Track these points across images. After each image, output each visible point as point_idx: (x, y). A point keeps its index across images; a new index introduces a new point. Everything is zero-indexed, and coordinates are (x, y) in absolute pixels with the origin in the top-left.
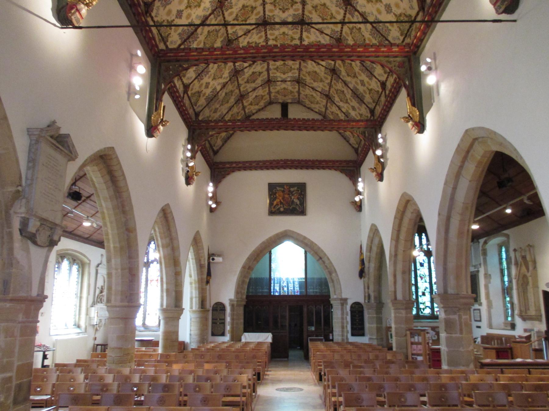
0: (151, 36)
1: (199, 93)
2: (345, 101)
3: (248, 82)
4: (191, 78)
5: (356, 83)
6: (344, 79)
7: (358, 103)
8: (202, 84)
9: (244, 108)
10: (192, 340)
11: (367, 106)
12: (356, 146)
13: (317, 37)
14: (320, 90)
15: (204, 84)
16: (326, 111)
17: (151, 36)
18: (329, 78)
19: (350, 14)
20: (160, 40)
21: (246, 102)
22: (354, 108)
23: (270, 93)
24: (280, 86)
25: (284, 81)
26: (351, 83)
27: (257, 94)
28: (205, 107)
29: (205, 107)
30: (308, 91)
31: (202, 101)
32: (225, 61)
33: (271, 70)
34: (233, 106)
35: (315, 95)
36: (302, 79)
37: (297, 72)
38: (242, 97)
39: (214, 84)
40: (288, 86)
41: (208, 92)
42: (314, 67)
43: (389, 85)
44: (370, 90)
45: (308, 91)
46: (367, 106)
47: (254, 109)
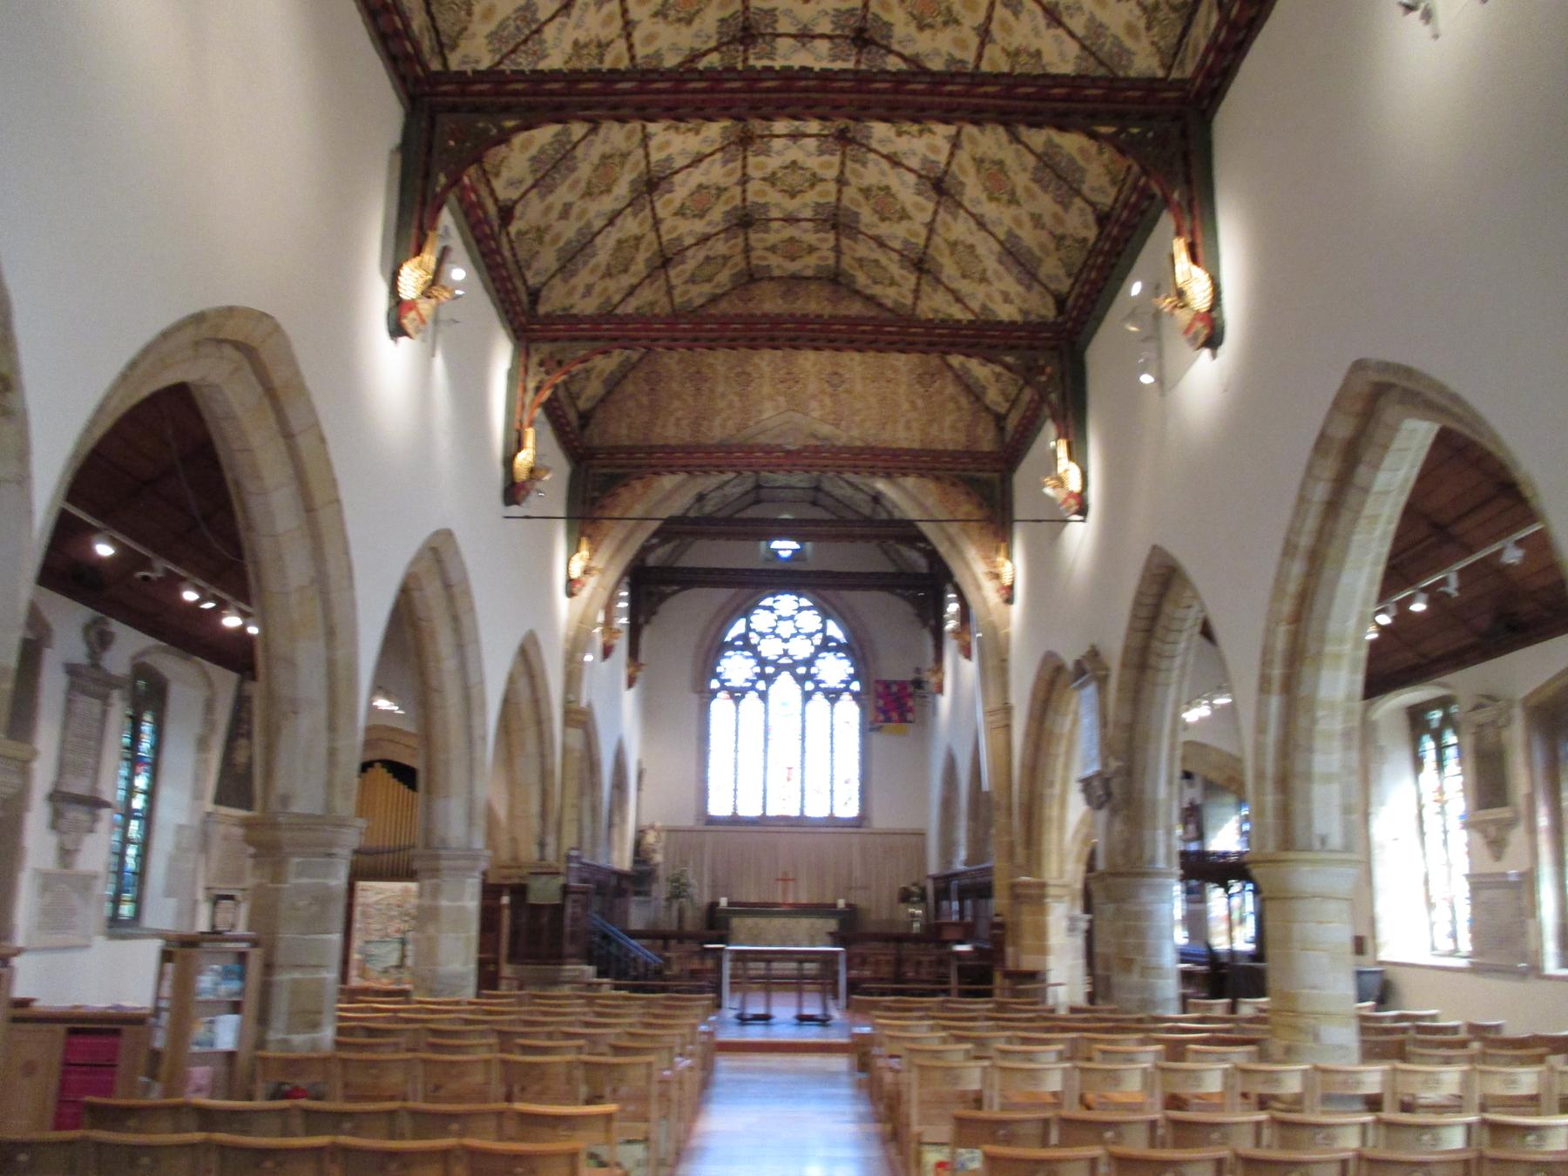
0: (399, 25)
1: (540, 232)
2: (1005, 197)
3: (692, 280)
4: (521, 182)
5: (988, 296)
6: (954, 285)
7: (1019, 282)
8: (574, 289)
9: (670, 290)
10: (164, 1004)
11: (1046, 287)
12: (1002, 410)
13: (883, 173)
14: (914, 163)
15: (558, 207)
16: (915, 304)
17: (399, 25)
18: (931, 206)
19: (1006, 5)
20: (432, 49)
21: (678, 276)
22: (1007, 298)
23: (747, 250)
24: (778, 233)
25: (791, 220)
26: (973, 295)
27: (711, 253)
28: (553, 276)
29: (553, 276)
30: (864, 250)
31: (548, 259)
32: (612, 71)
33: (753, 249)
34: (640, 284)
35: (884, 261)
36: (877, 17)
37: (832, 187)
38: (652, 184)
39: (605, 289)
40: (807, 234)
41: (569, 231)
42: (883, 173)
43: (1012, 421)
44: (1060, 239)
45: (864, 250)
46: (1046, 287)
47: (691, 233)
